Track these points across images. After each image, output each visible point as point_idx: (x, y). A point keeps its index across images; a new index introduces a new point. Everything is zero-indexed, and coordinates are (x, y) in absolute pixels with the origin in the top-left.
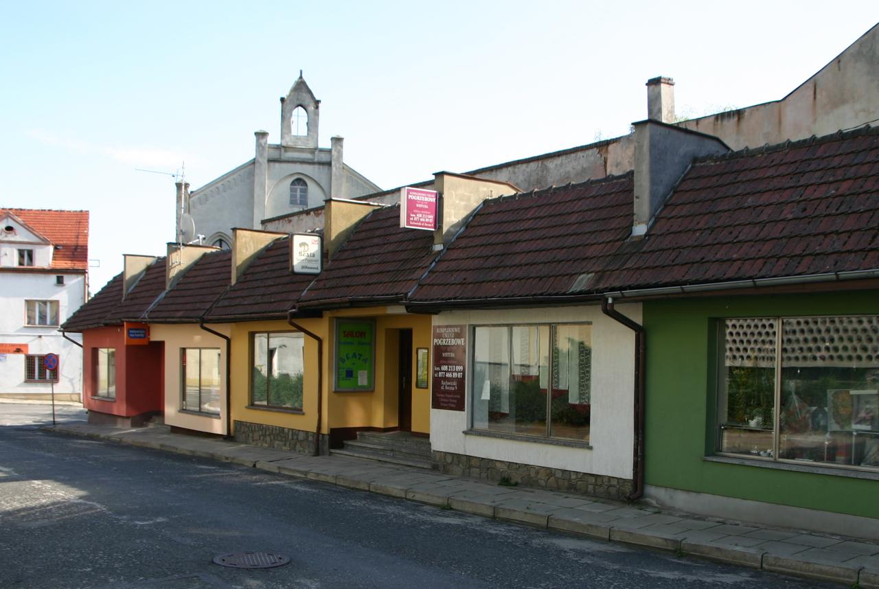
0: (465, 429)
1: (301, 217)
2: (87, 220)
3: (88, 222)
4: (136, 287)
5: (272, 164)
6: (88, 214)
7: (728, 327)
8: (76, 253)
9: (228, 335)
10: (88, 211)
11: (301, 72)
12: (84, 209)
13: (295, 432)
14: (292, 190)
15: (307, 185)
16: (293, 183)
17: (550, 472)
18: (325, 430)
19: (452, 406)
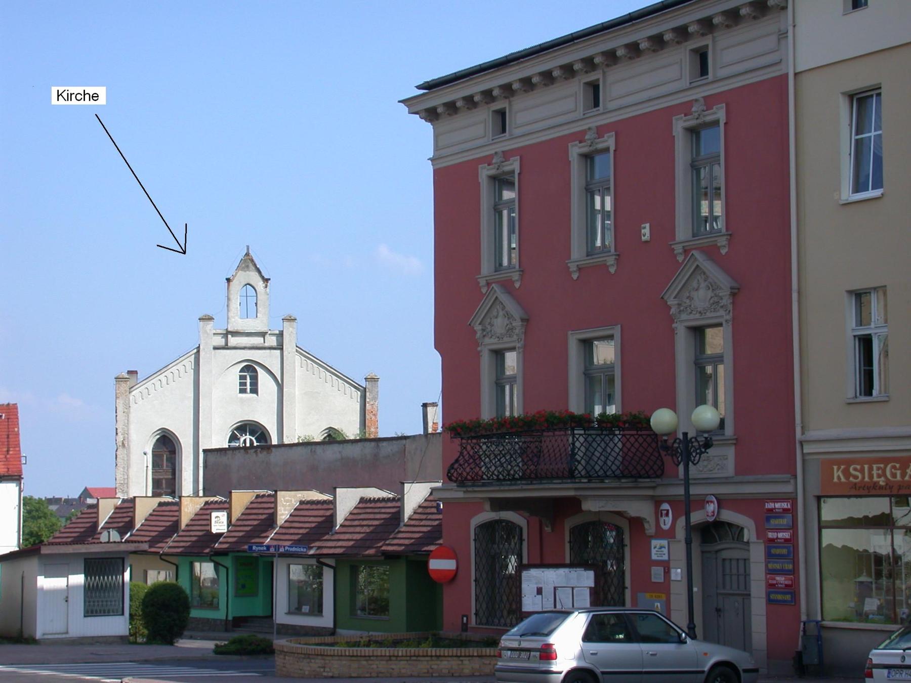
0: (286, 612)
1: (235, 452)
2: (17, 415)
3: (17, 418)
4: (106, 523)
5: (217, 351)
6: (17, 408)
7: (879, 482)
8: (8, 456)
9: (177, 563)
10: (16, 404)
11: (248, 247)
12: (12, 402)
13: (215, 620)
14: (242, 377)
15: (257, 372)
16: (242, 370)
17: (312, 628)
18: (230, 618)
19: (518, 598)
